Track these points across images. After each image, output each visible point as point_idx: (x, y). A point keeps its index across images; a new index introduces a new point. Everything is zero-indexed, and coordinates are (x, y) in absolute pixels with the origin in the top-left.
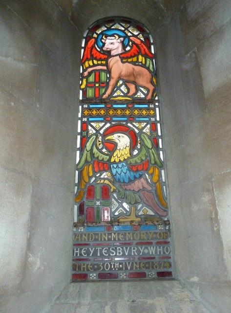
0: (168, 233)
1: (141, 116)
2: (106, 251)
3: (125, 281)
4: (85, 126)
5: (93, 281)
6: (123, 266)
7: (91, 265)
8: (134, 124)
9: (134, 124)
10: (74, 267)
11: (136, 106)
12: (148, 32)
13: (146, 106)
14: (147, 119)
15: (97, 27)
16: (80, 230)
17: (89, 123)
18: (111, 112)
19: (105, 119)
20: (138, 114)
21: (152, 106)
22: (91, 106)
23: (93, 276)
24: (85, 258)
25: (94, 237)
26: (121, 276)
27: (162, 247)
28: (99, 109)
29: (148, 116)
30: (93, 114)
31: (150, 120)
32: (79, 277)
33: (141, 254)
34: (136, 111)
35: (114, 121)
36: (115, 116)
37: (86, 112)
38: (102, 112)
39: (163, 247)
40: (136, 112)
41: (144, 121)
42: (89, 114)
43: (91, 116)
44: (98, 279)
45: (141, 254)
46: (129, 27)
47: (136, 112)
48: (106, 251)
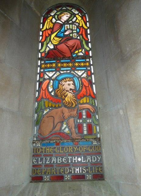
0: (100, 147)
1: (80, 66)
2: (36, 160)
3: (48, 182)
4: (42, 74)
5: (89, 180)
6: (72, 171)
7: (39, 170)
8: (76, 71)
9: (76, 71)
10: (33, 171)
11: (77, 60)
12: (85, 12)
13: (84, 60)
14: (85, 68)
15: (51, 11)
16: (38, 145)
17: (44, 73)
18: (59, 65)
19: (71, 68)
20: (78, 65)
21: (88, 60)
22: (47, 62)
23: (46, 178)
24: (36, 165)
25: (56, 149)
26: (87, 177)
27: (76, 157)
28: (51, 63)
29: (85, 66)
30: (47, 67)
31: (87, 69)
32: (36, 179)
33: (99, 161)
34: (77, 63)
35: (62, 71)
36: (62, 67)
37: (87, 64)
38: (54, 65)
39: (91, 157)
40: (77, 64)
41: (83, 70)
42: (46, 68)
43: (46, 68)
44: (50, 180)
45: (99, 161)
46: (72, 9)
47: (77, 64)
48: (65, 160)
